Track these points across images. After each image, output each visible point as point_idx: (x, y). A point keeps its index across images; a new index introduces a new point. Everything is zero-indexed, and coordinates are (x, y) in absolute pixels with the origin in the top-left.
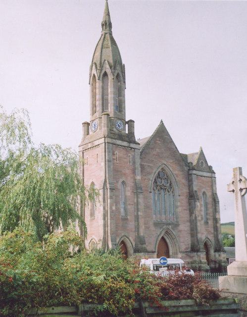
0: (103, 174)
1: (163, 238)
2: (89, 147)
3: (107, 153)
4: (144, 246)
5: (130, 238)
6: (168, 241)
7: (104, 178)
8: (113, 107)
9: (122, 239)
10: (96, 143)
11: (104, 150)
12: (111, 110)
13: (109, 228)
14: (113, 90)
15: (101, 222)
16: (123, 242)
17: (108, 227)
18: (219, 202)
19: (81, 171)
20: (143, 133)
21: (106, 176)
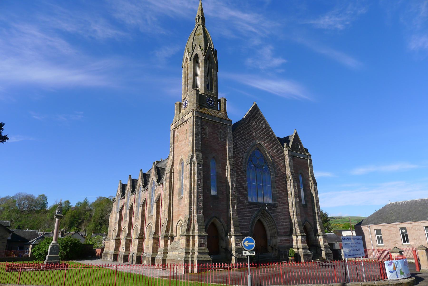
0: (190, 148)
1: (259, 220)
2: (179, 123)
3: (195, 127)
4: (233, 123)
5: (222, 219)
6: (265, 224)
7: (191, 152)
8: (203, 85)
9: (212, 221)
10: (186, 118)
11: (192, 124)
12: (201, 87)
13: (195, 207)
14: (203, 69)
15: (187, 200)
16: (213, 224)
17: (194, 205)
18: (33, 196)
19: (171, 149)
20: (236, 113)
21: (193, 151)
